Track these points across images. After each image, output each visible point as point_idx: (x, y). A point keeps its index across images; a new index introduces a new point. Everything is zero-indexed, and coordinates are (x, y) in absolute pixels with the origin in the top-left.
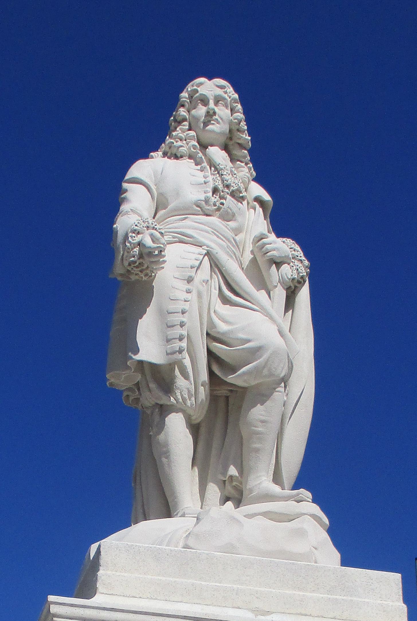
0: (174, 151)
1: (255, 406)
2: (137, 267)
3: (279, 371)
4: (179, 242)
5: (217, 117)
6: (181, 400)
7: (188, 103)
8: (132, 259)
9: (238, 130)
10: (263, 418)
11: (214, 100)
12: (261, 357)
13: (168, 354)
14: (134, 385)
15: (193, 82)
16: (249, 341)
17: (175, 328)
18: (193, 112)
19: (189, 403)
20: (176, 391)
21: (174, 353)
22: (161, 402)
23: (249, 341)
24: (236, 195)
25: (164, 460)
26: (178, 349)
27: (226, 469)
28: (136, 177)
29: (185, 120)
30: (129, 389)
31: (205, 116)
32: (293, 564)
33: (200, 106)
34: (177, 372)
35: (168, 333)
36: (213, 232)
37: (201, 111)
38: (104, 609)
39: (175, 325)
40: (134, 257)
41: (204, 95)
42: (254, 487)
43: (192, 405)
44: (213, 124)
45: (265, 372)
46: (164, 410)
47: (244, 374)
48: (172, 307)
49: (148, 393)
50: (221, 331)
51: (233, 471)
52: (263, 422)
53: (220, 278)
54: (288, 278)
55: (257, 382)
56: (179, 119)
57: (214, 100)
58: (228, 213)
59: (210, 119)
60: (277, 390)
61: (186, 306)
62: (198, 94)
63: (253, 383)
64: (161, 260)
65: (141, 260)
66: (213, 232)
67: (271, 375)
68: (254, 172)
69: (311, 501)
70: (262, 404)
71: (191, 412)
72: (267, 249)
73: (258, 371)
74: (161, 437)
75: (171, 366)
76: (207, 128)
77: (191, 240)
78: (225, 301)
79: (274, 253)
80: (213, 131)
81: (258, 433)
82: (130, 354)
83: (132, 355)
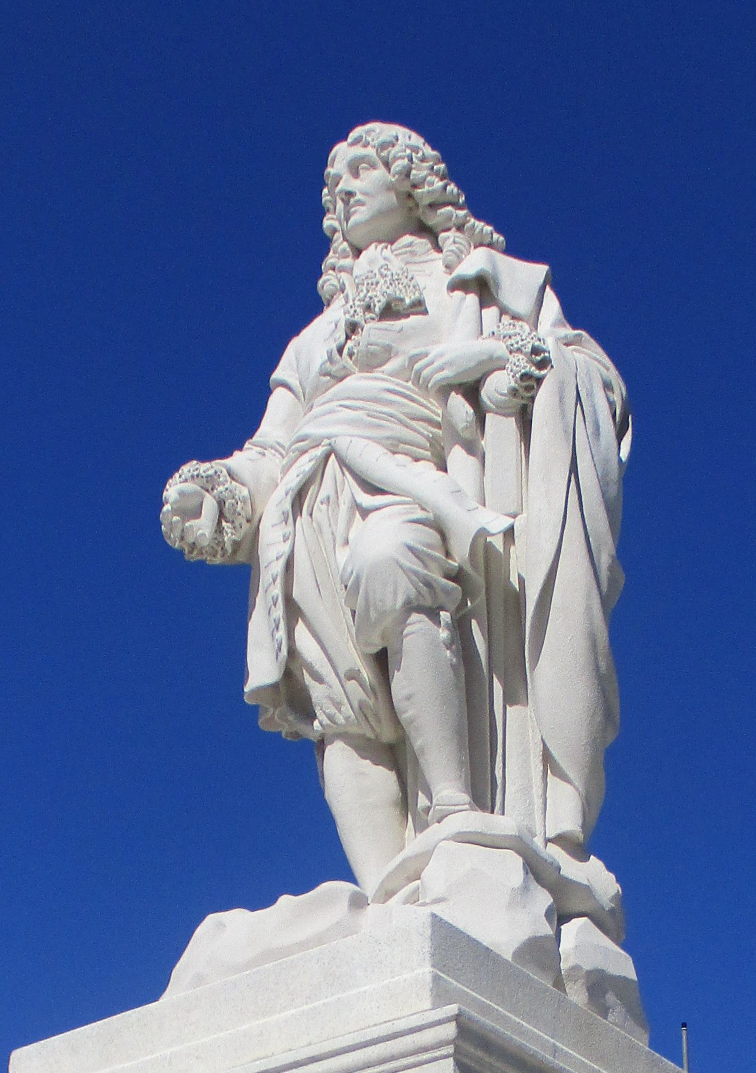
3: (389, 604)
4: (302, 455)
5: (359, 196)
9: (415, 186)
11: (374, 162)
19: (340, 719)
24: (401, 308)
29: (335, 231)
32: (281, 964)
36: (341, 406)
43: (347, 719)
54: (502, 395)
57: (374, 162)
58: (373, 354)
60: (405, 632)
66: (341, 406)
67: (382, 614)
68: (479, 225)
69: (467, 806)
71: (354, 730)
74: (611, 738)
77: (306, 442)
79: (447, 373)
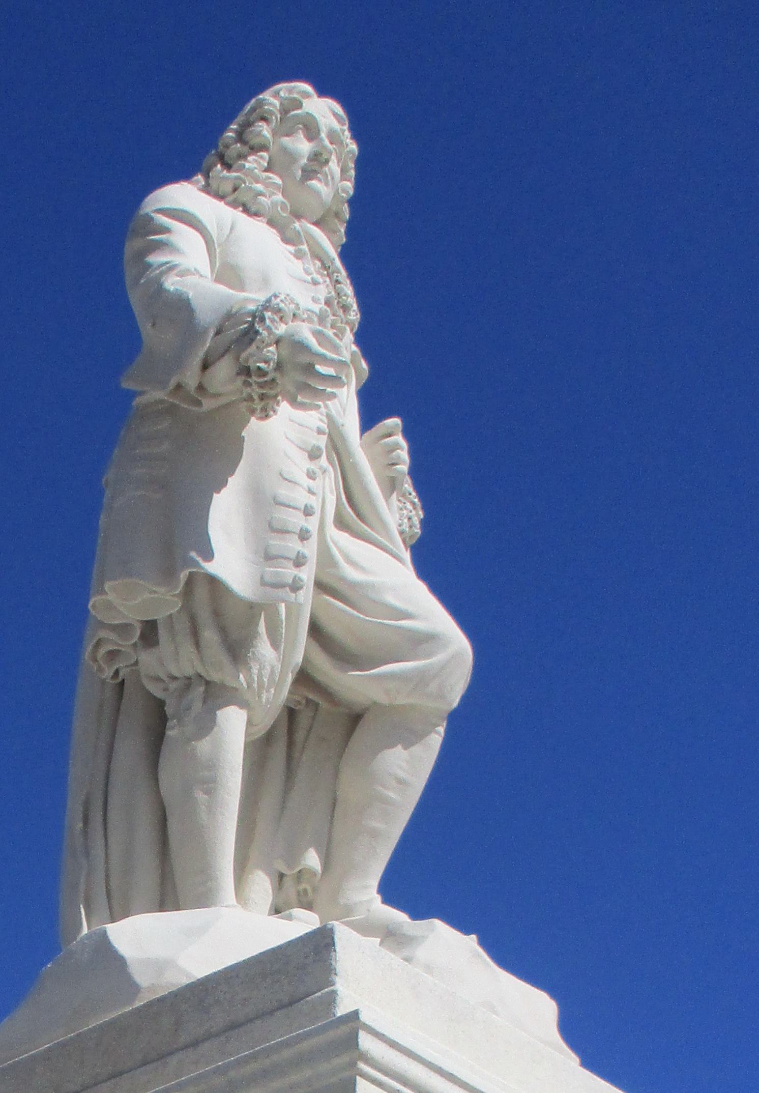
0: (245, 197)
1: (392, 746)
2: (261, 385)
6: (255, 685)
7: (276, 118)
8: (262, 365)
10: (402, 774)
12: (429, 655)
13: (263, 583)
14: (138, 621)
15: (293, 84)
16: (407, 616)
17: (287, 536)
18: (286, 141)
20: (252, 664)
21: (282, 586)
22: (215, 676)
23: (407, 616)
25: (201, 796)
26: (290, 581)
27: (293, 854)
28: (181, 207)
29: (264, 148)
30: (123, 629)
31: (310, 159)
33: (301, 135)
34: (262, 628)
35: (272, 542)
37: (303, 146)
38: (393, 1045)
39: (287, 532)
40: (266, 362)
41: (314, 118)
42: (355, 904)
44: (320, 180)
45: (433, 687)
46: (216, 695)
47: (393, 676)
48: (284, 492)
49: (191, 649)
50: (343, 579)
51: (312, 860)
52: (401, 782)
53: (339, 474)
55: (411, 701)
56: (255, 141)
59: (316, 168)
61: (314, 502)
62: (299, 112)
63: (401, 700)
64: (329, 390)
65: (277, 375)
70: (405, 749)
72: (399, 457)
73: (419, 680)
74: (203, 746)
75: (252, 609)
76: (309, 182)
78: (341, 523)
80: (317, 194)
81: (385, 801)
82: (193, 554)
83: (199, 559)
